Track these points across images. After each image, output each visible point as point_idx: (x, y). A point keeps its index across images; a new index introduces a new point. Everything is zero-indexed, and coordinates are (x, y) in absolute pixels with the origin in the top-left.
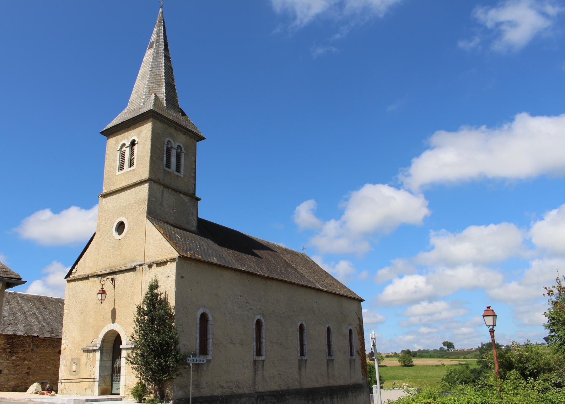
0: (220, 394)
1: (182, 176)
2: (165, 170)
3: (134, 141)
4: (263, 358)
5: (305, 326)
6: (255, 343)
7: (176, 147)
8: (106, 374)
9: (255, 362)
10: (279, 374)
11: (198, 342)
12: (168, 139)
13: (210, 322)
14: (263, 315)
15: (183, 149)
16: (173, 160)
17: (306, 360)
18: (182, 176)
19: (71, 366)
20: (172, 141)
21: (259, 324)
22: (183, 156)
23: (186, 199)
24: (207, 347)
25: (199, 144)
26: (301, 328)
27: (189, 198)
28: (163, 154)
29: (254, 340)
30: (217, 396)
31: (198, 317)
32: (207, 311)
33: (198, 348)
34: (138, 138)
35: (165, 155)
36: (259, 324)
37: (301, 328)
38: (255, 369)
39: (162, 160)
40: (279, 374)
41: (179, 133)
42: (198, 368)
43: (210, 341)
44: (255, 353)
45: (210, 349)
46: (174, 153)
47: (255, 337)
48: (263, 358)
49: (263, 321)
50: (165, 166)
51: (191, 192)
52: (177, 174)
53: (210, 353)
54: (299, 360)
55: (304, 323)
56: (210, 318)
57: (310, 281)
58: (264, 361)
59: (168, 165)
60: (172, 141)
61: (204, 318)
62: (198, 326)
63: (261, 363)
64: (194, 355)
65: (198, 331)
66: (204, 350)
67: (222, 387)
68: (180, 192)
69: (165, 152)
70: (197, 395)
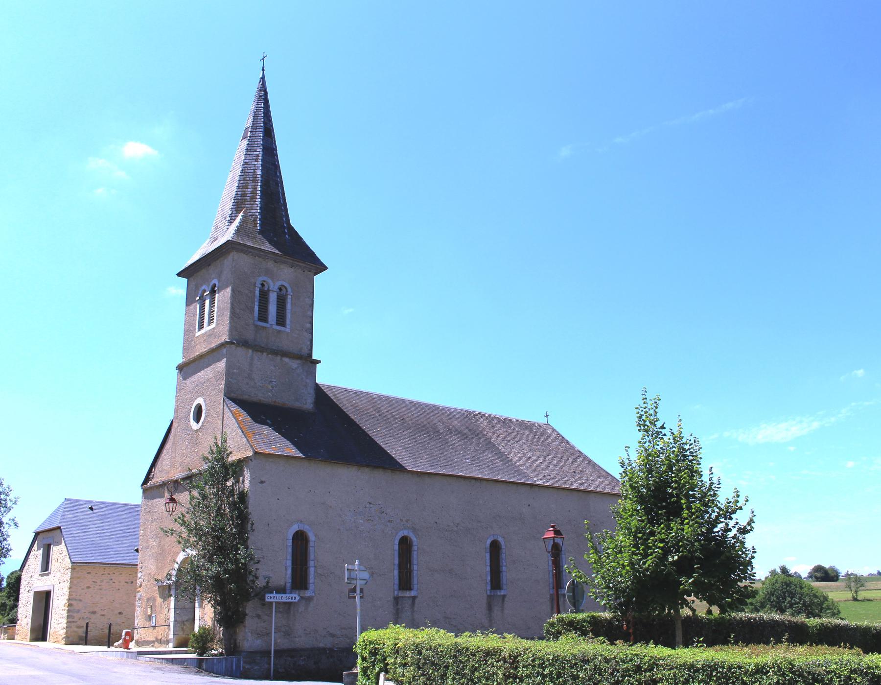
0: (329, 646)
1: (288, 330)
2: (256, 326)
3: (215, 286)
4: (502, 593)
5: (502, 543)
6: (396, 572)
7: (276, 288)
8: (185, 618)
9: (397, 599)
10: (446, 618)
11: (289, 571)
12: (261, 278)
13: (311, 544)
14: (414, 530)
15: (289, 290)
16: (272, 309)
17: (504, 596)
18: (288, 330)
19: (146, 608)
20: (270, 281)
21: (405, 545)
22: (289, 301)
23: (294, 364)
24: (499, 581)
25: (318, 279)
26: (495, 548)
27: (299, 362)
28: (253, 302)
29: (396, 568)
30: (324, 649)
31: (290, 536)
32: (306, 528)
33: (290, 581)
34: (219, 281)
35: (257, 303)
36: (405, 545)
37: (495, 548)
38: (398, 609)
39: (252, 310)
40: (446, 618)
41: (282, 267)
42: (289, 608)
43: (312, 570)
44: (396, 587)
45: (311, 581)
46: (273, 298)
47: (397, 562)
48: (502, 593)
49: (414, 539)
50: (256, 319)
51: (305, 351)
52: (279, 328)
53: (311, 587)
54: (489, 597)
55: (500, 539)
56: (312, 537)
57: (519, 472)
58: (414, 598)
59: (263, 316)
60: (270, 281)
61: (300, 539)
62: (290, 550)
63: (410, 602)
64: (281, 590)
65: (289, 557)
66: (300, 581)
67: (333, 636)
68: (284, 354)
69: (257, 299)
70: (285, 644)
